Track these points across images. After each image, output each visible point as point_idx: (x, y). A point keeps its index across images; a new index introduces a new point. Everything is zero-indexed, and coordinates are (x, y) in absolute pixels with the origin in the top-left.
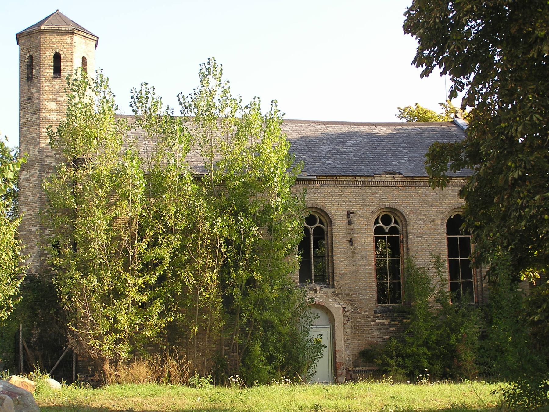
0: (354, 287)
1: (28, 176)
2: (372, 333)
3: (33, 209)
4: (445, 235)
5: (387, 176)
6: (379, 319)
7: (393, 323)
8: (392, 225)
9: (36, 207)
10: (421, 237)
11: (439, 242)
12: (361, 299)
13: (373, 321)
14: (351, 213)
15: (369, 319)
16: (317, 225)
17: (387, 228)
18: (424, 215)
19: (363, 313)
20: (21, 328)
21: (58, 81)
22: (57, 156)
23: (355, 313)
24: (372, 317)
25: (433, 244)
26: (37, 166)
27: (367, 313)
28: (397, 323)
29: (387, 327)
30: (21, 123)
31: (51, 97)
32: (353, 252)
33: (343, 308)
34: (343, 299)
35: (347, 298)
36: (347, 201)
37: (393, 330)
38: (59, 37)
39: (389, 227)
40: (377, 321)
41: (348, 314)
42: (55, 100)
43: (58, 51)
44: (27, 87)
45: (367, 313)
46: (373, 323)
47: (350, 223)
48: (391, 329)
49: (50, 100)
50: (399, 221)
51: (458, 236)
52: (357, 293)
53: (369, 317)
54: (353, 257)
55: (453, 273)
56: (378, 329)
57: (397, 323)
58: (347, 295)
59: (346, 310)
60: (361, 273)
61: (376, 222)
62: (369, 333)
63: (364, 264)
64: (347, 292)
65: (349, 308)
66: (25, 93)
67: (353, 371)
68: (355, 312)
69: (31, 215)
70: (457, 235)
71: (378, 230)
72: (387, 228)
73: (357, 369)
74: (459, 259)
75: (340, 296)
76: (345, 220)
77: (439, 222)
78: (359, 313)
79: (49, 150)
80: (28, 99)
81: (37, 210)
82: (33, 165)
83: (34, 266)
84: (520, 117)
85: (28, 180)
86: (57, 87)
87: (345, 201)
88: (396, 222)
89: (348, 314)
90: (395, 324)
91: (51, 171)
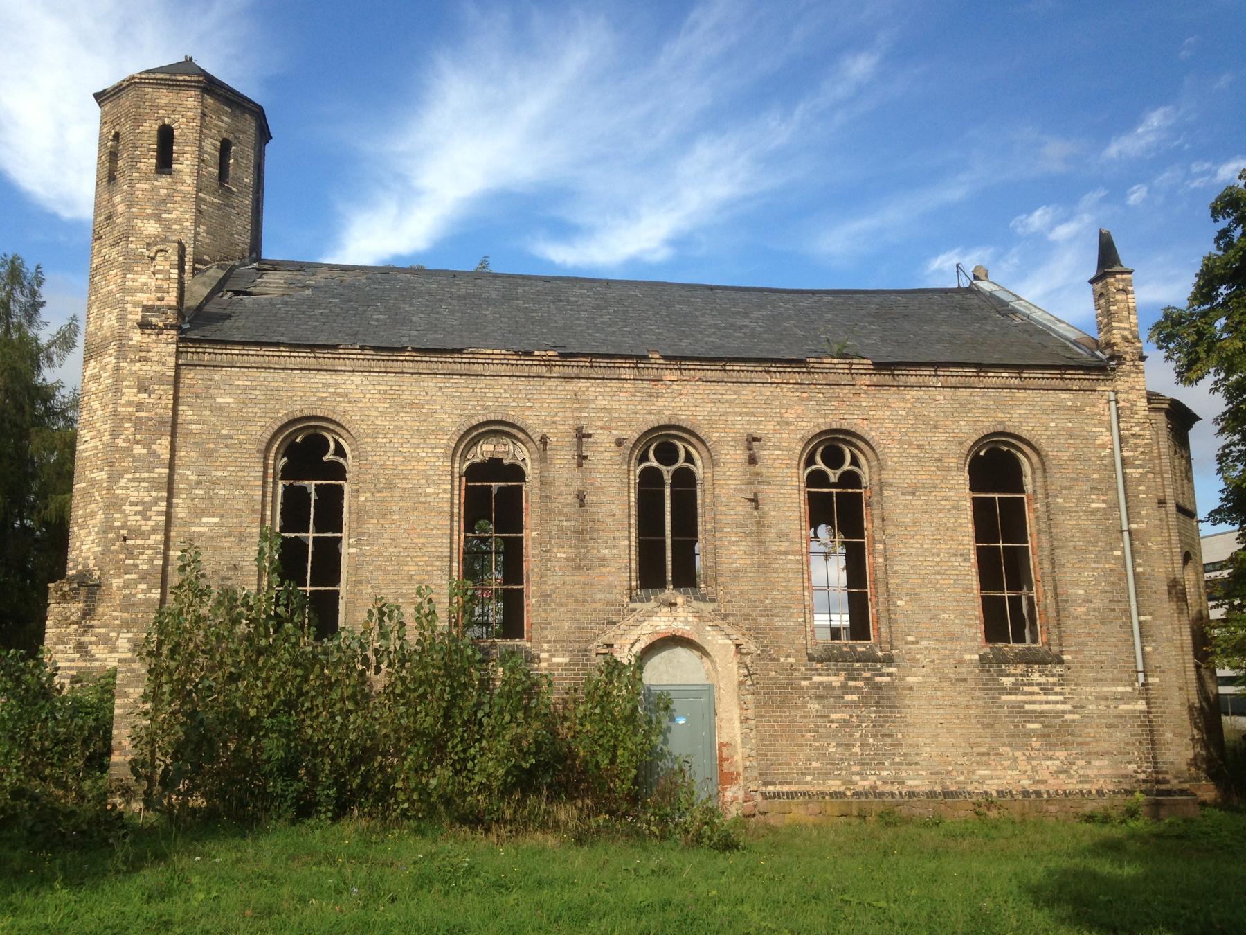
0: (761, 601)
2: (804, 706)
3: (99, 435)
4: (967, 490)
5: (835, 361)
6: (820, 675)
7: (851, 683)
8: (847, 466)
9: (105, 430)
10: (914, 494)
11: (953, 507)
12: (777, 629)
13: (805, 679)
14: (755, 439)
15: (796, 674)
16: (654, 463)
17: (833, 475)
18: (919, 447)
19: (782, 660)
21: (164, 180)
23: (763, 659)
24: (803, 669)
25: (940, 511)
26: (112, 349)
27: (791, 660)
28: (861, 684)
29: (839, 692)
31: (149, 211)
32: (759, 524)
33: (737, 646)
34: (735, 625)
35: (745, 625)
36: (747, 414)
37: (853, 702)
38: (173, 95)
39: (839, 472)
40: (816, 679)
41: (748, 659)
42: (158, 218)
43: (167, 121)
44: (106, 196)
45: (791, 660)
46: (805, 683)
47: (752, 460)
48: (848, 697)
49: (149, 217)
50: (862, 460)
51: (997, 496)
52: (768, 613)
53: (795, 670)
54: (759, 533)
56: (816, 697)
57: (861, 684)
58: (747, 617)
59: (744, 651)
60: (776, 571)
61: (810, 461)
62: (797, 707)
63: (783, 549)
64: (746, 611)
65: (750, 646)
67: (763, 794)
68: (765, 656)
70: (993, 492)
71: (816, 479)
72: (833, 475)
73: (771, 788)
74: (1001, 545)
75: (731, 619)
76: (741, 455)
77: (953, 462)
78: (773, 660)
80: (107, 219)
82: (106, 348)
83: (93, 553)
85: (95, 378)
86: (163, 192)
87: (741, 414)
88: (855, 462)
89: (748, 659)
90: (856, 688)
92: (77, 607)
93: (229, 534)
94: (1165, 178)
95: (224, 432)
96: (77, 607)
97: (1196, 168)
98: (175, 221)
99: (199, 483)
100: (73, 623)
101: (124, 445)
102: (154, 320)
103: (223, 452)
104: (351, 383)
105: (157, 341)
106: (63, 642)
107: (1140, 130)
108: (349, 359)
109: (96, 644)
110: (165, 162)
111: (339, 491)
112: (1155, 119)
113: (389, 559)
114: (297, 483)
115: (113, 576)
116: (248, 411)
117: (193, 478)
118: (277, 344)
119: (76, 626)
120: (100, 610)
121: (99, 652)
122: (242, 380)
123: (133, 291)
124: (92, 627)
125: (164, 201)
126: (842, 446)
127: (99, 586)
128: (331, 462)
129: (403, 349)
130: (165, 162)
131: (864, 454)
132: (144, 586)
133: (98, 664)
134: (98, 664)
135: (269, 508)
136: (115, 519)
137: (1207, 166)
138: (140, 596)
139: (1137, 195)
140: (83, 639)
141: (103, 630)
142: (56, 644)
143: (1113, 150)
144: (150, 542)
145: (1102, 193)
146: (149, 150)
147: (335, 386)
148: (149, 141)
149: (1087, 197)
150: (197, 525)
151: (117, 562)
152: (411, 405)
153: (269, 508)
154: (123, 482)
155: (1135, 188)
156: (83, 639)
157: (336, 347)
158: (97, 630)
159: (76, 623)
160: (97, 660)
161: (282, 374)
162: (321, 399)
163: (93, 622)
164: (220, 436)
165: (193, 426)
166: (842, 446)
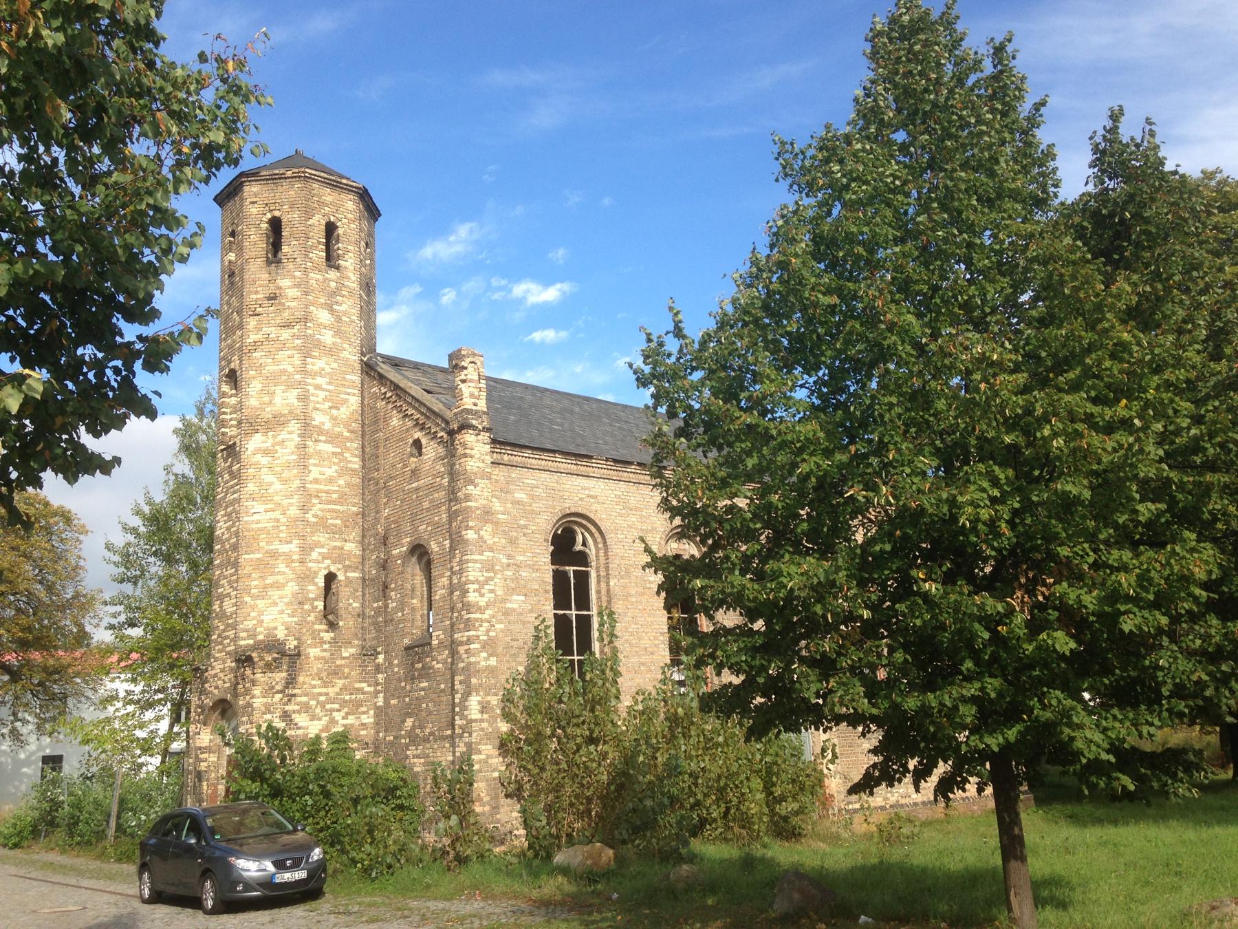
1: (269, 444)
9: (290, 505)
20: (1191, 479)
21: (333, 274)
22: (334, 412)
30: (239, 333)
38: (335, 194)
43: (332, 219)
55: (561, 599)
66: (260, 286)
69: (277, 521)
79: (320, 399)
80: (269, 298)
81: (294, 512)
84: (1018, 288)
86: (333, 284)
91: (323, 438)
92: (280, 676)
93: (531, 611)
94: (472, 285)
95: (522, 522)
96: (280, 676)
97: (495, 282)
98: (345, 313)
99: (508, 565)
100: (278, 692)
101: (315, 520)
102: (474, 422)
103: (523, 540)
104: (598, 487)
105: (478, 441)
106: (270, 712)
107: (452, 238)
108: (598, 468)
109: (299, 712)
110: (331, 259)
111: (587, 574)
112: (463, 231)
113: (632, 634)
114: (561, 568)
115: (311, 646)
116: (537, 506)
117: (505, 561)
118: (554, 452)
119: (280, 695)
120: (301, 679)
121: (301, 719)
122: (530, 478)
123: (314, 375)
124: (294, 695)
125: (334, 294)
126: (576, 528)
127: (299, 655)
128: (580, 552)
129: (631, 463)
130: (331, 259)
131: (592, 535)
132: (484, 655)
133: (300, 732)
134: (300, 732)
135: (604, 591)
136: (309, 592)
137: (504, 282)
138: (483, 663)
139: (448, 296)
140: (287, 708)
141: (304, 699)
142: (264, 713)
143: (428, 252)
144: (486, 616)
145: (418, 289)
146: (320, 243)
147: (589, 489)
148: (319, 235)
149: (405, 290)
150: (511, 602)
151: (313, 632)
152: (636, 509)
153: (604, 591)
154: (314, 555)
155: (447, 290)
156: (287, 708)
157: (591, 457)
158: (299, 699)
159: (281, 692)
160: (299, 728)
161: (556, 476)
162: (581, 499)
163: (295, 691)
164: (519, 526)
165: (500, 516)
166: (576, 528)
